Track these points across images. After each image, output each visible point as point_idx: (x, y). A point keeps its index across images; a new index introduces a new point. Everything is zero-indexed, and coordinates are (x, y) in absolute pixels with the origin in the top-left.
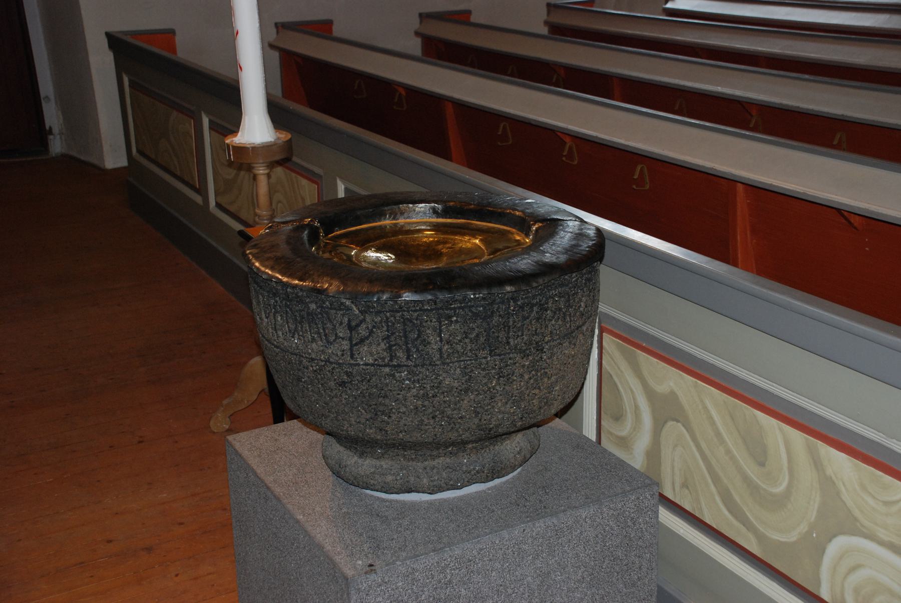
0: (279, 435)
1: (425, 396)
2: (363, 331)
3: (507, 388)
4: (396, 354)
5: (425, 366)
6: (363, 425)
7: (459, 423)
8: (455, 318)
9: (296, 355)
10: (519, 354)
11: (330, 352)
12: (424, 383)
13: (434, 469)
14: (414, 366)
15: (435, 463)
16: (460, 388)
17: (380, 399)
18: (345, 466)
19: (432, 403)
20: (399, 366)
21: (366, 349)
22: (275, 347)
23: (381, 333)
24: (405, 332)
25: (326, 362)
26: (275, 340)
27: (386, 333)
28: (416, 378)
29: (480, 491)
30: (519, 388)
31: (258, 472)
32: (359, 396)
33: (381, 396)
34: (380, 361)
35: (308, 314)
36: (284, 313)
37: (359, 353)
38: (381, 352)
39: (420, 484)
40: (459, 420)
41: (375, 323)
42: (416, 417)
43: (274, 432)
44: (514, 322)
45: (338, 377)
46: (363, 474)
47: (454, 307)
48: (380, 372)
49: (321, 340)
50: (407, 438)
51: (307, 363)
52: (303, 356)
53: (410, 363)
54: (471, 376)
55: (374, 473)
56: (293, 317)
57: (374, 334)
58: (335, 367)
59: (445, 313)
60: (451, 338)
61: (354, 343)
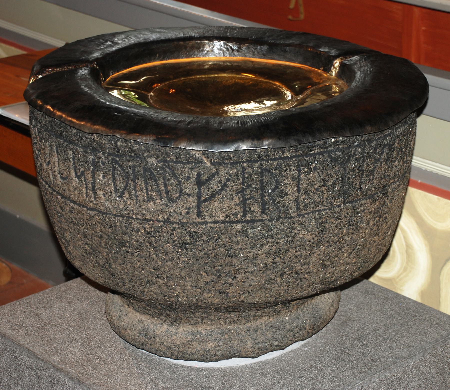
0: (38, 308)
1: (278, 253)
2: (215, 185)
3: (354, 236)
4: (250, 209)
5: (280, 220)
6: (200, 289)
7: (306, 278)
8: (314, 165)
9: (123, 216)
10: (368, 200)
11: (172, 211)
12: (278, 238)
13: (257, 330)
14: (269, 221)
15: (258, 322)
16: (312, 241)
17: (228, 259)
18: (154, 337)
19: (283, 259)
20: (253, 221)
21: (216, 205)
22: (88, 209)
23: (234, 186)
24: (261, 182)
25: (164, 222)
26: (92, 202)
27: (241, 185)
28: (270, 233)
29: (295, 350)
30: (364, 236)
31: (37, 352)
32: (202, 258)
33: (229, 256)
34: (232, 217)
35: (145, 170)
36: (109, 170)
37: (208, 210)
38: (234, 207)
39: (244, 348)
40: (306, 276)
41: (230, 175)
42: (264, 275)
43: (30, 306)
44: (368, 165)
45: (178, 238)
46: (178, 343)
47: (314, 153)
48: (231, 230)
49: (161, 198)
50: (250, 300)
51: (138, 225)
52: (132, 218)
53: (264, 217)
54: (325, 227)
55: (191, 341)
56: (124, 175)
57: (227, 187)
58: (175, 228)
59: (305, 160)
60: (309, 187)
61: (203, 199)
